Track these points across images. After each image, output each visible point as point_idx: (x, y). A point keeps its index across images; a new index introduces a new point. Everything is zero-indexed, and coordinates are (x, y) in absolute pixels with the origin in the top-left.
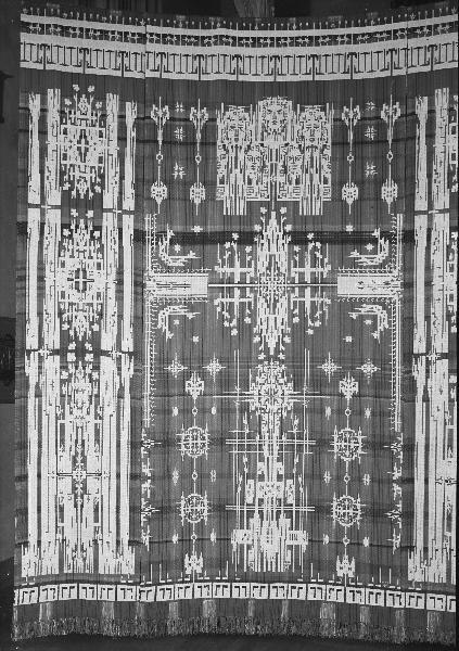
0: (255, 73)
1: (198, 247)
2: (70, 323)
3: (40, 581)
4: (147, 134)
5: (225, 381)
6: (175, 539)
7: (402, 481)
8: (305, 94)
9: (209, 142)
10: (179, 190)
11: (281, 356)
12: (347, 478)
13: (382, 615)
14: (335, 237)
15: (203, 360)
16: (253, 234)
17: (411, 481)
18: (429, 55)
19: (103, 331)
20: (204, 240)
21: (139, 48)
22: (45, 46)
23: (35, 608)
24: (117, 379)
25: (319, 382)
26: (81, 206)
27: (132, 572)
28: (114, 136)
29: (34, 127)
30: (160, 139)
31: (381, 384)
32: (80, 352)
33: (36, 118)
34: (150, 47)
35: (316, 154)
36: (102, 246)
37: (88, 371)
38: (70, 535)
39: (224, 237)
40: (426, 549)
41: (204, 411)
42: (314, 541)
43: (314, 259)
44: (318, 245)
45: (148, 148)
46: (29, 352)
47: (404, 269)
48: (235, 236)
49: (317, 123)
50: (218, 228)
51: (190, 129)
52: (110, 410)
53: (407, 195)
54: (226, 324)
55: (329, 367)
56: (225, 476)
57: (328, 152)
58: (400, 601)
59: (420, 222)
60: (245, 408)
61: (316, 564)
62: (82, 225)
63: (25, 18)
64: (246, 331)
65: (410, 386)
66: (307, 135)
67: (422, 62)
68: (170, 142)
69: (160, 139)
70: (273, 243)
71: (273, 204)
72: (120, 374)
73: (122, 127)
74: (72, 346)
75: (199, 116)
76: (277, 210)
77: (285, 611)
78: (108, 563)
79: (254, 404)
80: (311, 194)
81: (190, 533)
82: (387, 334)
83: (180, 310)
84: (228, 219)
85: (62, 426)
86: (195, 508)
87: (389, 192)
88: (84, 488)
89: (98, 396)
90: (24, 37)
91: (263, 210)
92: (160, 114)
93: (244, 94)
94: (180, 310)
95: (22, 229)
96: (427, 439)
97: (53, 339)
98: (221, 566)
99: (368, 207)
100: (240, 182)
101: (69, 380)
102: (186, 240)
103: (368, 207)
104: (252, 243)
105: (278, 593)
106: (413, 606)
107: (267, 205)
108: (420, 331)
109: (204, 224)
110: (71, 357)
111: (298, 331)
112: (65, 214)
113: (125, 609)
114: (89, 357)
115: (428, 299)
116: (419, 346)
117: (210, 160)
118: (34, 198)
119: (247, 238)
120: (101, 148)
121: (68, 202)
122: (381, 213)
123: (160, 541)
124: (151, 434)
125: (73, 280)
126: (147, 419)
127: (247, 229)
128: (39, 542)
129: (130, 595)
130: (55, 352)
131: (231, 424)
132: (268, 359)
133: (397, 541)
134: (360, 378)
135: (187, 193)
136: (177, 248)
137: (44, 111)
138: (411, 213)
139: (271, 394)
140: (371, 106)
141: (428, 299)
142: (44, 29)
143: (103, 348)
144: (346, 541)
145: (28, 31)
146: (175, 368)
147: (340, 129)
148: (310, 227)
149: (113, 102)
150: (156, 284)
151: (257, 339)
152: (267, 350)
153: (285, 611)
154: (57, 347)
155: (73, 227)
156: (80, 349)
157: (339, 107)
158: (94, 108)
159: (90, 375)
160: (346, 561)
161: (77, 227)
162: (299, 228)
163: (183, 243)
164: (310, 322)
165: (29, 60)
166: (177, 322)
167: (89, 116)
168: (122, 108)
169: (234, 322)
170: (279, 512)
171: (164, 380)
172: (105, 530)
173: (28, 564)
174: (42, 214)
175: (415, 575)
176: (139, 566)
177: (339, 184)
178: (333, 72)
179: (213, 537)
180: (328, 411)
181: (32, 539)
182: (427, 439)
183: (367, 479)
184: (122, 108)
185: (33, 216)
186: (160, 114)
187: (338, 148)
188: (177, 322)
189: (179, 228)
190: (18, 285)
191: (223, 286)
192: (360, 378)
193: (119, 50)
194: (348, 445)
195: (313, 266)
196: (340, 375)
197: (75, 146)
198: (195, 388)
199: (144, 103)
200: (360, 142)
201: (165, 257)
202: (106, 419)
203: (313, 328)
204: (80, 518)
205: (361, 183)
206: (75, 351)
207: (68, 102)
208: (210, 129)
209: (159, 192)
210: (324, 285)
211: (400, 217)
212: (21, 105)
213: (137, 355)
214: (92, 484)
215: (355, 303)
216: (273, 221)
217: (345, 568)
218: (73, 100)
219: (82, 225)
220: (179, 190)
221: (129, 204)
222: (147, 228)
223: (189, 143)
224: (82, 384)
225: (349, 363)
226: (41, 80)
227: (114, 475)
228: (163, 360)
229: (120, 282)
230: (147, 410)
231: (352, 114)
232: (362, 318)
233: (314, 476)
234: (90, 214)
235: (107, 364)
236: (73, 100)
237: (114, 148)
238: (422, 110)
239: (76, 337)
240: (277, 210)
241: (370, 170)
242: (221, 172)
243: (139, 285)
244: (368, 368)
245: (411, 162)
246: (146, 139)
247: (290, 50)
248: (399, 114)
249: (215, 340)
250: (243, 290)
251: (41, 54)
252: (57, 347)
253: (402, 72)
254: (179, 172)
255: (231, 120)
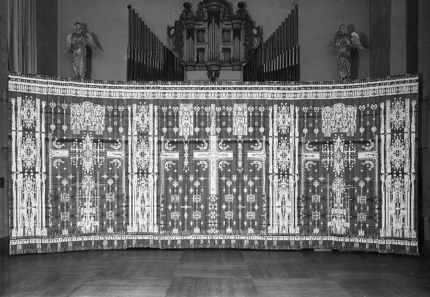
0: (334, 96)
1: (317, 145)
2: (281, 166)
3: (17, 238)
4: (49, 110)
5: (74, 180)
6: (59, 225)
7: (126, 206)
8: (348, 102)
9: (68, 113)
10: (311, 130)
11: (342, 176)
12: (316, 207)
13: (372, 246)
14: (357, 142)
15: (319, 176)
16: (82, 139)
17: (128, 206)
18: (384, 91)
19: (405, 167)
20: (318, 143)
21: (46, 86)
22: (16, 84)
23: (16, 246)
24: (410, 181)
25: (353, 183)
26: (29, 131)
27: (46, 235)
28: (39, 111)
29: (13, 108)
30: (362, 115)
31: (119, 182)
32: (29, 173)
33: (14, 106)
34: (49, 86)
35: (100, 118)
36: (35, 142)
37: (32, 177)
38: (27, 225)
39: (325, 143)
40: (273, 225)
41: (67, 189)
42: (102, 224)
43: (100, 147)
44: (352, 144)
45: (49, 115)
46: (382, 174)
47: (125, 151)
48: (76, 140)
49: (352, 110)
50: (71, 138)
51: (62, 110)
52: (38, 189)
53: (126, 131)
54: (74, 164)
55: (105, 176)
56: (75, 207)
57: (355, 118)
58: (125, 238)
59: (130, 138)
60: (331, 190)
61: (102, 231)
62: (398, 138)
63: (10, 76)
64: (81, 167)
65: (268, 182)
66: (349, 114)
67: (382, 93)
68: (56, 113)
69: (362, 115)
70: (88, 142)
71: (339, 134)
72: (411, 179)
73: (41, 109)
74: (26, 171)
75: (316, 109)
76: (89, 133)
77: (93, 244)
78: (39, 233)
79: (334, 189)
80: (99, 128)
81: (315, 222)
82: (262, 169)
83: (60, 160)
84: (326, 138)
85: (279, 194)
86: (316, 216)
87: (121, 130)
88: (31, 212)
89: (35, 185)
90: (10, 82)
91: (336, 135)
92: (53, 105)
93: (331, 103)
94: (60, 160)
95: (10, 137)
96: (273, 196)
97: (20, 169)
98: (74, 231)
99: (115, 133)
100: (78, 125)
101: (25, 180)
102: (313, 144)
103: (115, 133)
104: (332, 144)
105: (92, 238)
106: (382, 243)
107: (86, 131)
108: (383, 167)
109: (318, 139)
110: (26, 174)
111: (347, 169)
112: (24, 133)
113: (44, 246)
114: (32, 174)
115: (273, 159)
116: (130, 171)
117: (68, 119)
118: (13, 128)
119: (80, 141)
120: (404, 115)
121: (24, 129)
122: (372, 136)
123: (166, 224)
124: (51, 195)
125: (25, 152)
126: (50, 191)
127: (80, 138)
128: (17, 227)
129: (46, 241)
130: (390, 174)
131: (76, 192)
132: (337, 176)
133: (124, 223)
134: (365, 182)
135: (61, 127)
136: (170, 145)
137: (16, 103)
138: (127, 136)
139: (338, 187)
140: (368, 105)
141: (273, 159)
142: (16, 80)
143: (149, 172)
144: (362, 225)
145: (11, 80)
146: (59, 177)
147: (359, 112)
148: (99, 138)
149: (38, 100)
150: (53, 153)
151: (83, 169)
152: (337, 174)
153: (93, 244)
154: (22, 171)
155: (395, 139)
156: (29, 172)
157: (358, 106)
158: (32, 103)
159: (401, 180)
160: (65, 230)
161: (396, 138)
162: (347, 140)
163: (61, 142)
164: (99, 164)
165: (11, 88)
166: (59, 164)
167: (400, 106)
168: (41, 103)
169: (77, 164)
170: (91, 217)
171: (55, 181)
172: (38, 223)
173: (14, 233)
174: (17, 135)
175: (382, 235)
176: (48, 233)
177: (106, 127)
178: (357, 95)
179: (322, 223)
180: (105, 188)
181: (15, 226)
182: (273, 196)
183: (59, 207)
184: (41, 103)
185: (13, 133)
186: (374, 107)
187: (358, 117)
188: (59, 164)
189: (60, 137)
190: (9, 153)
191: (72, 153)
192: (365, 182)
193: (40, 86)
194: (110, 197)
195: (100, 149)
196: (108, 179)
197: (28, 113)
198: (65, 182)
199: (48, 102)
200: (365, 115)
201: (167, 148)
202: (406, 192)
203: (351, 168)
204: (284, 219)
205: (113, 126)
206: (141, 173)
207: (24, 101)
208: (68, 110)
209: (305, 131)
210: (103, 154)
211: (377, 136)
212: (9, 101)
213: (159, 174)
214: (147, 208)
215: (112, 159)
216: (339, 138)
217: (110, 230)
218: (394, 103)
219: (398, 138)
220: (311, 130)
221: (43, 130)
222: (303, 141)
223: (227, 116)
224: (284, 182)
225: (197, 176)
226: (15, 95)
227: (152, 206)
228: (55, 175)
229: (41, 153)
230: (50, 189)
231: (110, 108)
232: (114, 163)
233: (352, 208)
234: (31, 133)
235: (38, 176)
236: (394, 103)
237: (408, 115)
238: (382, 106)
239: (283, 170)
240: (89, 133)
241: (115, 123)
242: (323, 125)
243: (47, 153)
244: (368, 179)
245: (127, 122)
246: (301, 116)
247: (321, 91)
248: (376, 107)
249: (320, 170)
250: (330, 157)
251: (397, 90)
252: (22, 171)
253: (378, 95)
254: (59, 121)
255: (326, 111)
